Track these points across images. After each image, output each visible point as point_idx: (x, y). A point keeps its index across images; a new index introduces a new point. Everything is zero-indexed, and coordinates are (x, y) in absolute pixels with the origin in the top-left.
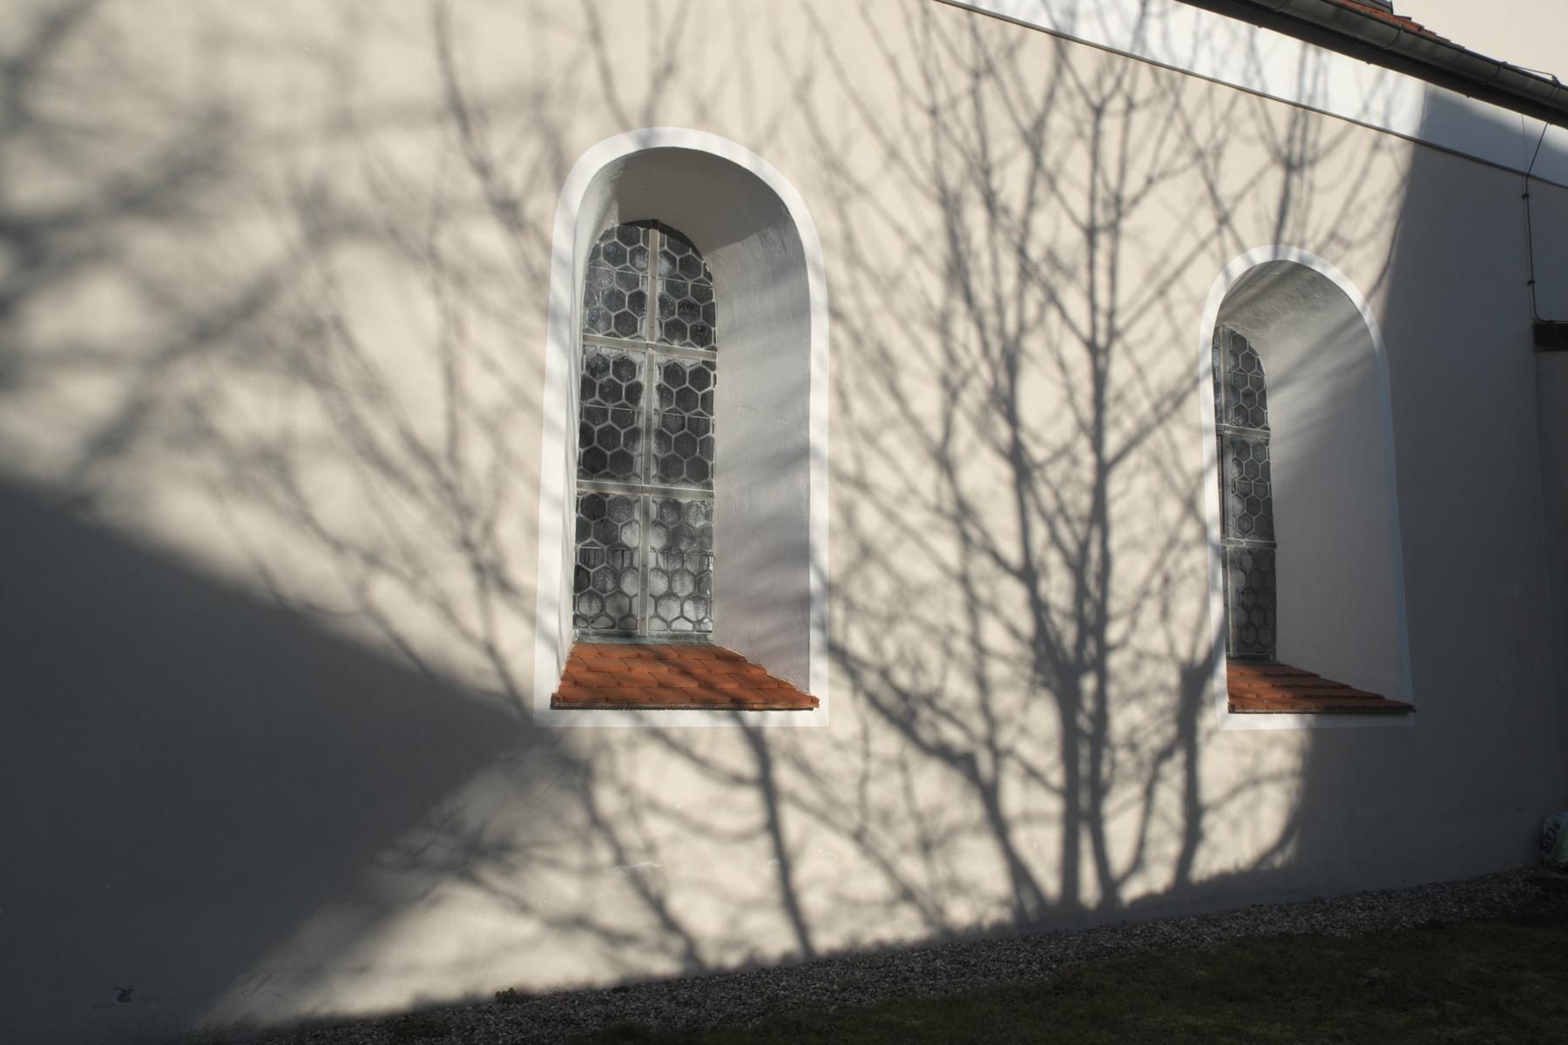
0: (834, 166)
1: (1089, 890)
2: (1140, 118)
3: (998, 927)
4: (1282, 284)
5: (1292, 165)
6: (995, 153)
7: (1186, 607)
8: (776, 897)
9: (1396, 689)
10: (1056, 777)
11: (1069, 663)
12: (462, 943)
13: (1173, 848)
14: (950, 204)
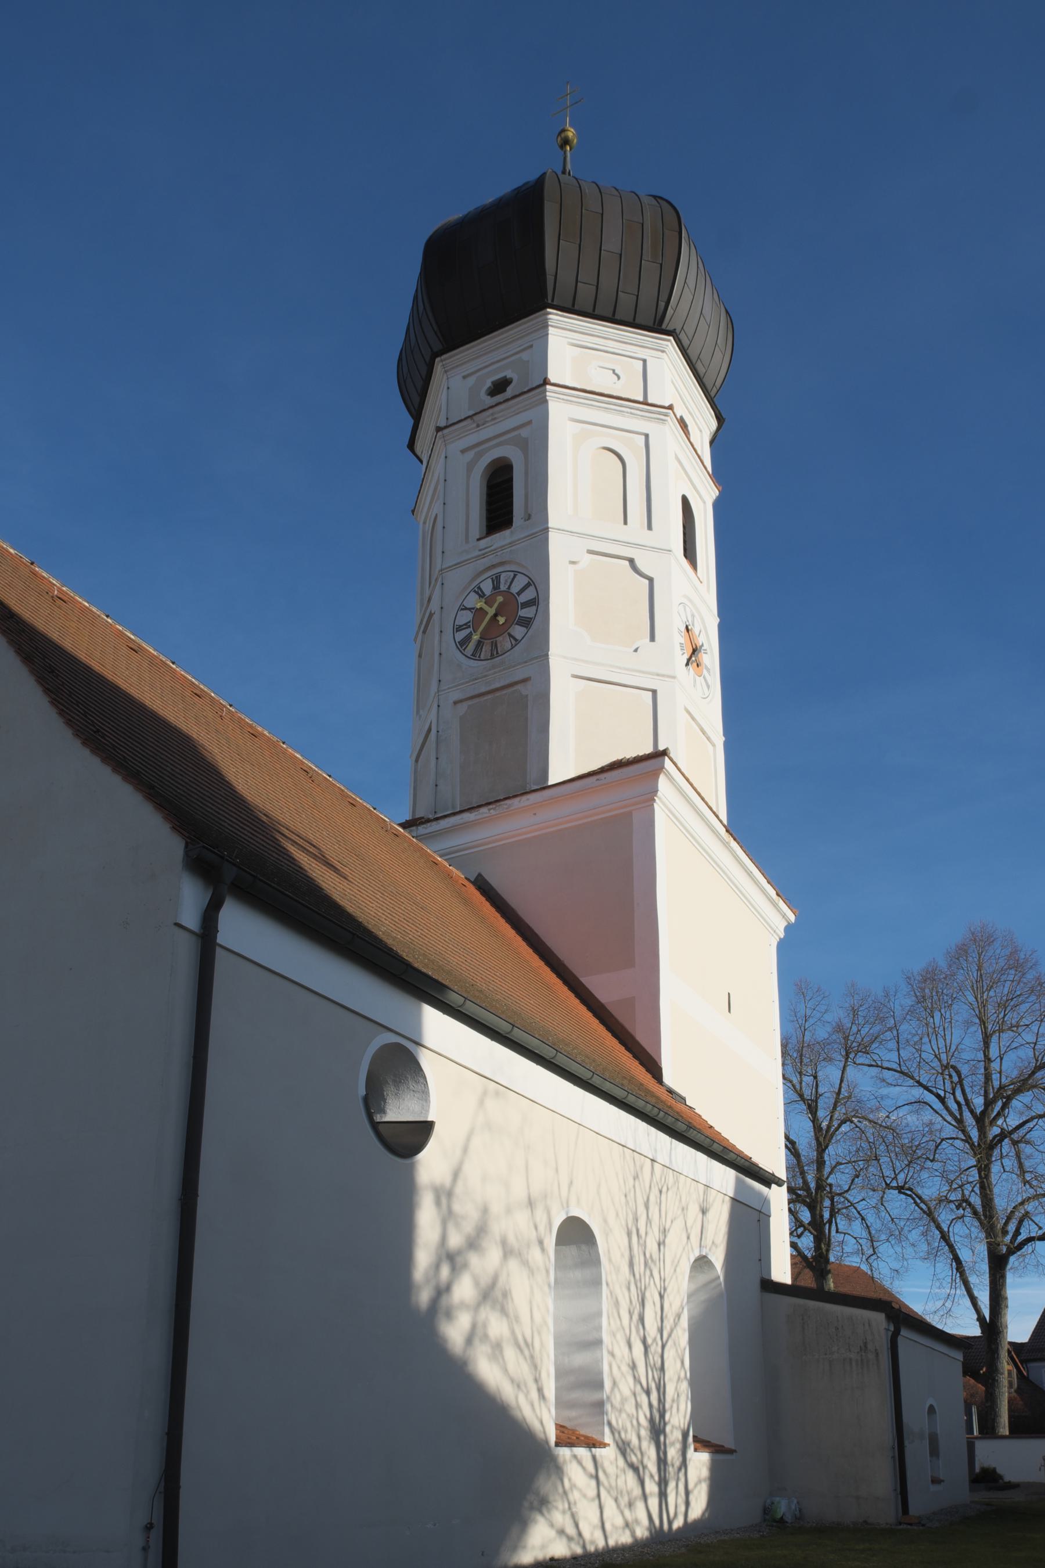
0: (605, 1221)
1: (666, 1526)
2: (670, 1193)
3: (647, 1539)
4: (702, 1262)
5: (704, 1212)
6: (639, 1213)
7: (682, 1407)
8: (600, 1524)
9: (729, 1444)
10: (657, 1478)
11: (657, 1431)
12: (543, 1538)
13: (682, 1508)
14: (629, 1234)
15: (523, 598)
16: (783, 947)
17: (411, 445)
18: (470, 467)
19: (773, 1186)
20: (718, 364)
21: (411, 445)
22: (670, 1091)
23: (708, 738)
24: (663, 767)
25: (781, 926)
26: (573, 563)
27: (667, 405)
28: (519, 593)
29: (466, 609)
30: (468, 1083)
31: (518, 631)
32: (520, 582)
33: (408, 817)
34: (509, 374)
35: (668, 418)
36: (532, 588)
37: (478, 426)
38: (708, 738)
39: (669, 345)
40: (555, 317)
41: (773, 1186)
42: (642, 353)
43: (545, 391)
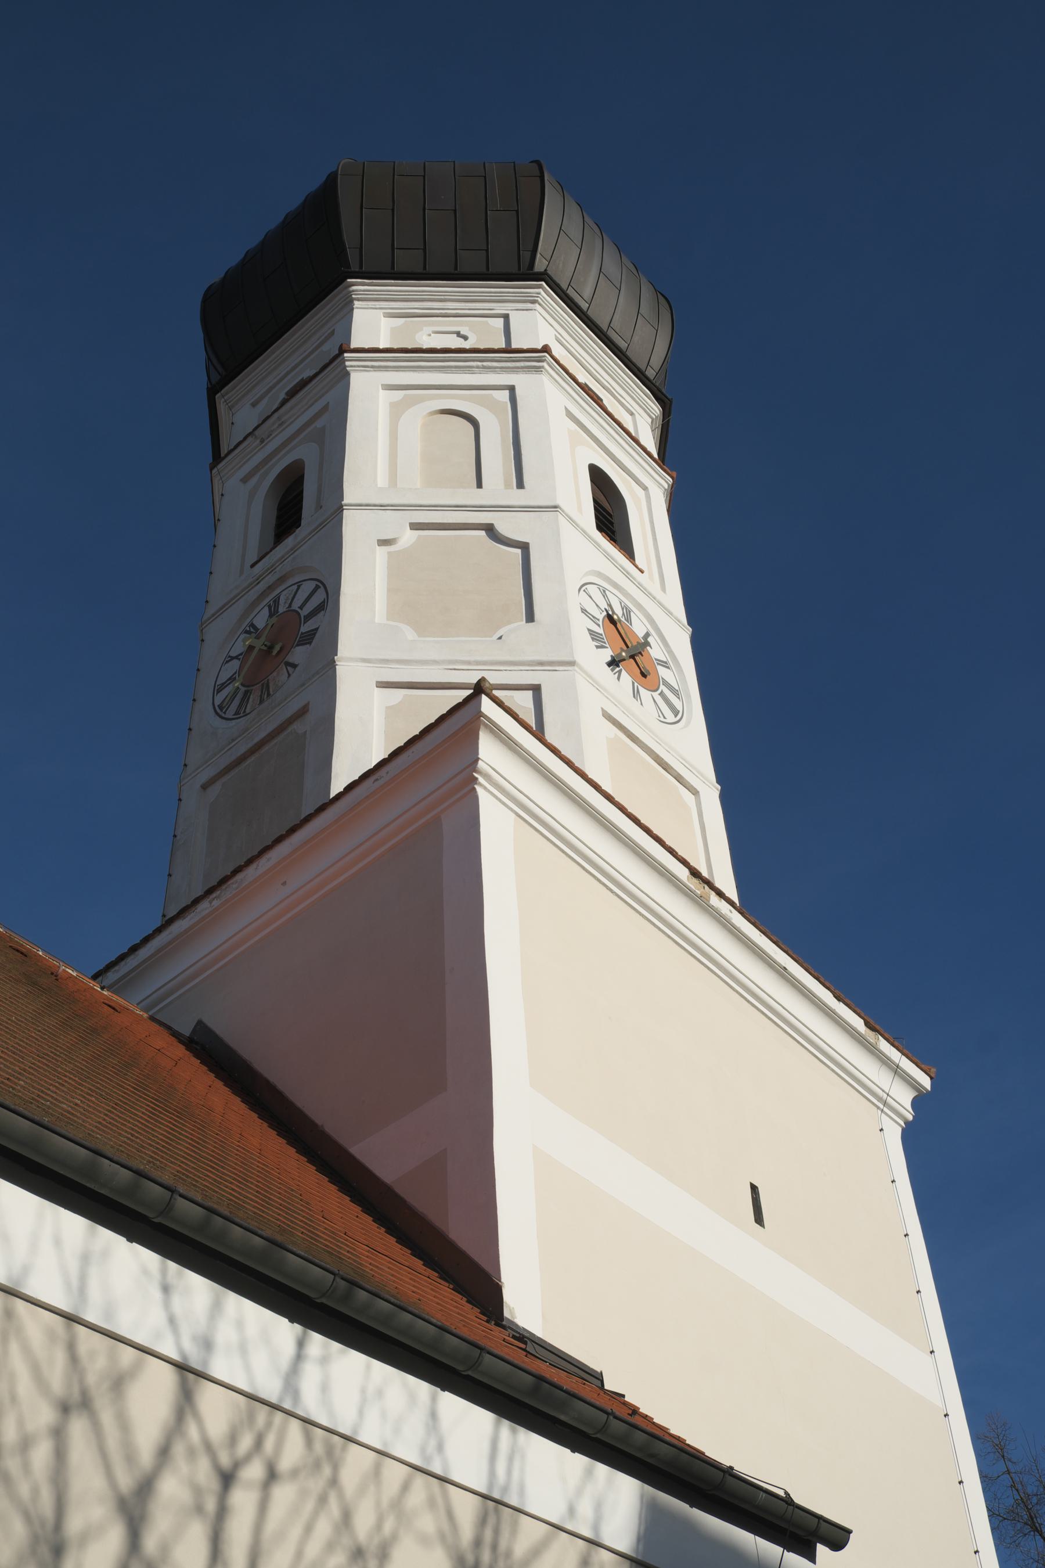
2: (283, 1494)
16: (915, 1139)
19: (821, 1550)
20: (654, 346)
23: (679, 779)
24: (480, 714)
25: (904, 1098)
26: (383, 543)
27: (540, 347)
28: (301, 608)
29: (232, 658)
35: (545, 364)
36: (321, 590)
37: (262, 441)
38: (679, 779)
39: (543, 293)
40: (359, 287)
41: (821, 1550)
42: (500, 308)
43: (344, 360)
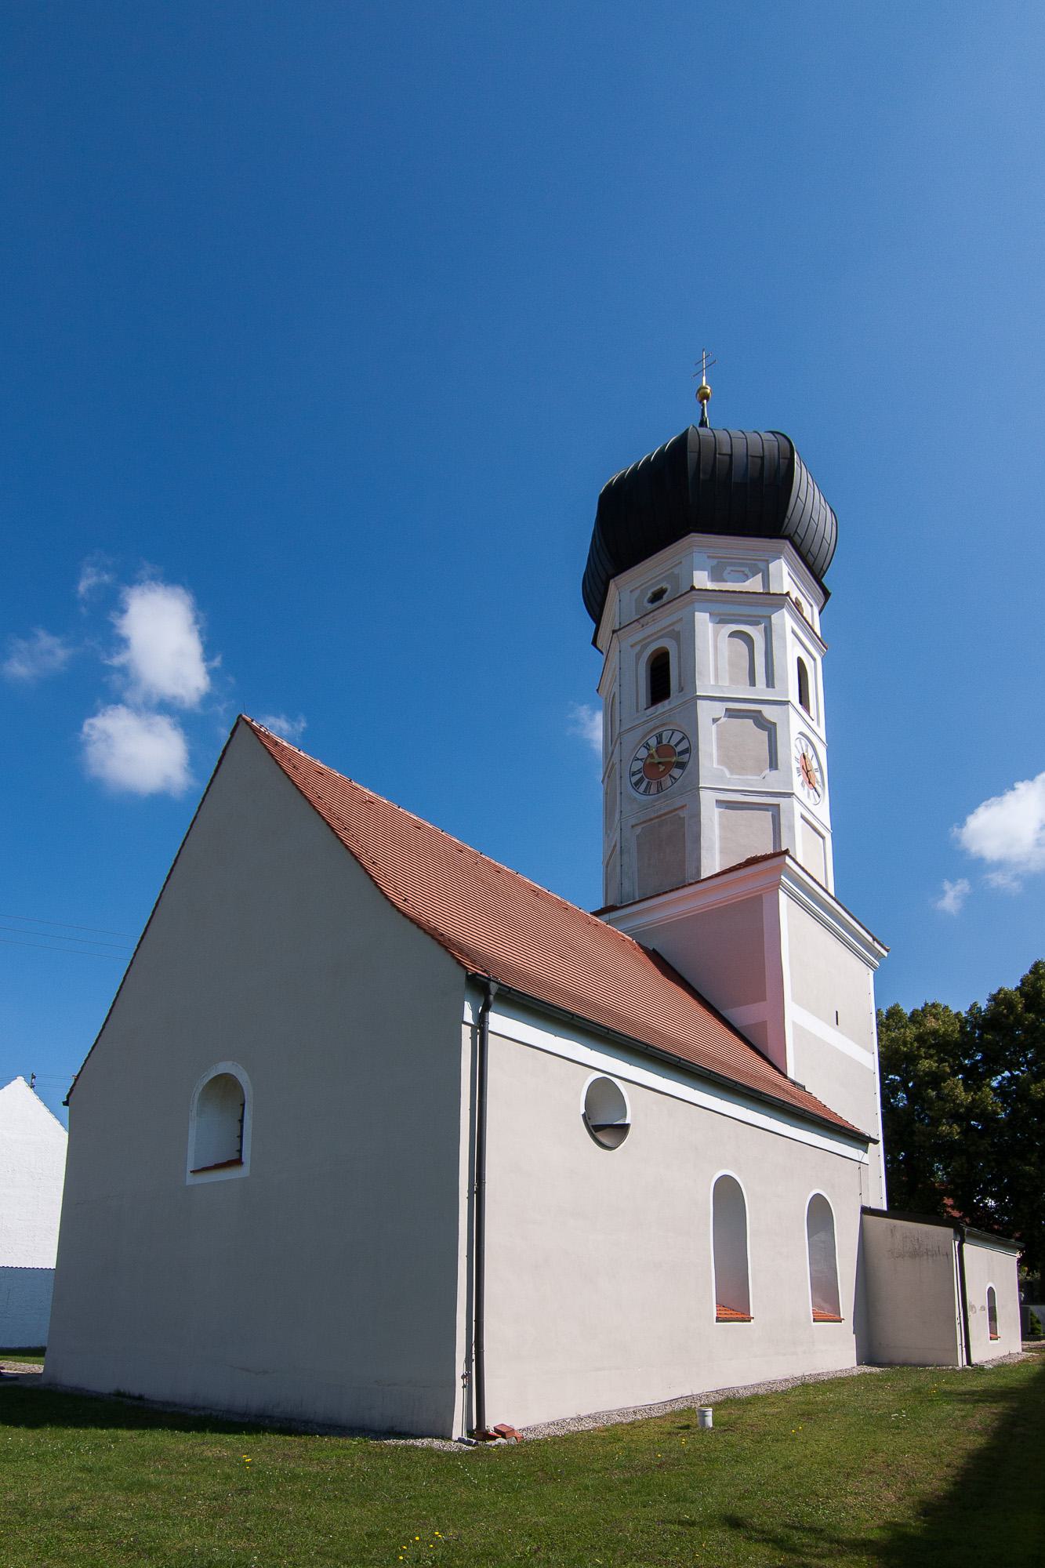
15: (679, 749)
17: (594, 643)
18: (638, 656)
21: (594, 643)
22: (794, 1083)
30: (531, 1077)
31: (676, 772)
32: (677, 737)
33: (601, 905)
34: (664, 585)
